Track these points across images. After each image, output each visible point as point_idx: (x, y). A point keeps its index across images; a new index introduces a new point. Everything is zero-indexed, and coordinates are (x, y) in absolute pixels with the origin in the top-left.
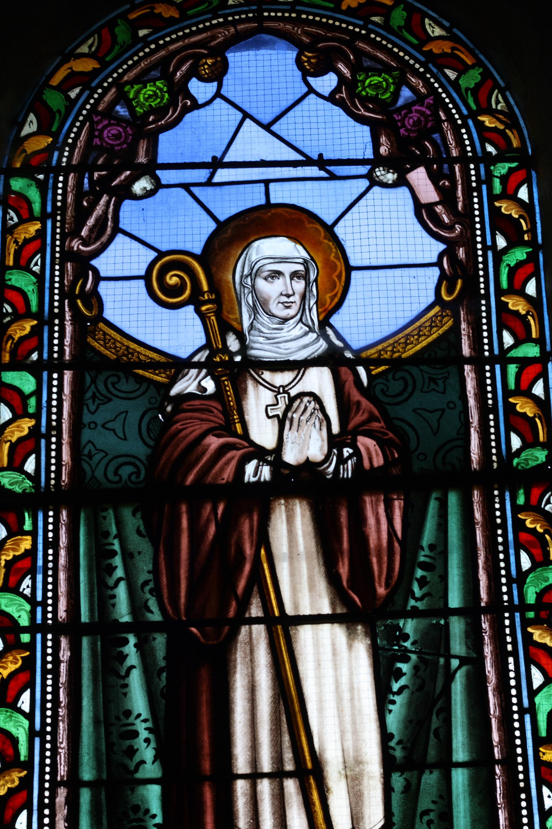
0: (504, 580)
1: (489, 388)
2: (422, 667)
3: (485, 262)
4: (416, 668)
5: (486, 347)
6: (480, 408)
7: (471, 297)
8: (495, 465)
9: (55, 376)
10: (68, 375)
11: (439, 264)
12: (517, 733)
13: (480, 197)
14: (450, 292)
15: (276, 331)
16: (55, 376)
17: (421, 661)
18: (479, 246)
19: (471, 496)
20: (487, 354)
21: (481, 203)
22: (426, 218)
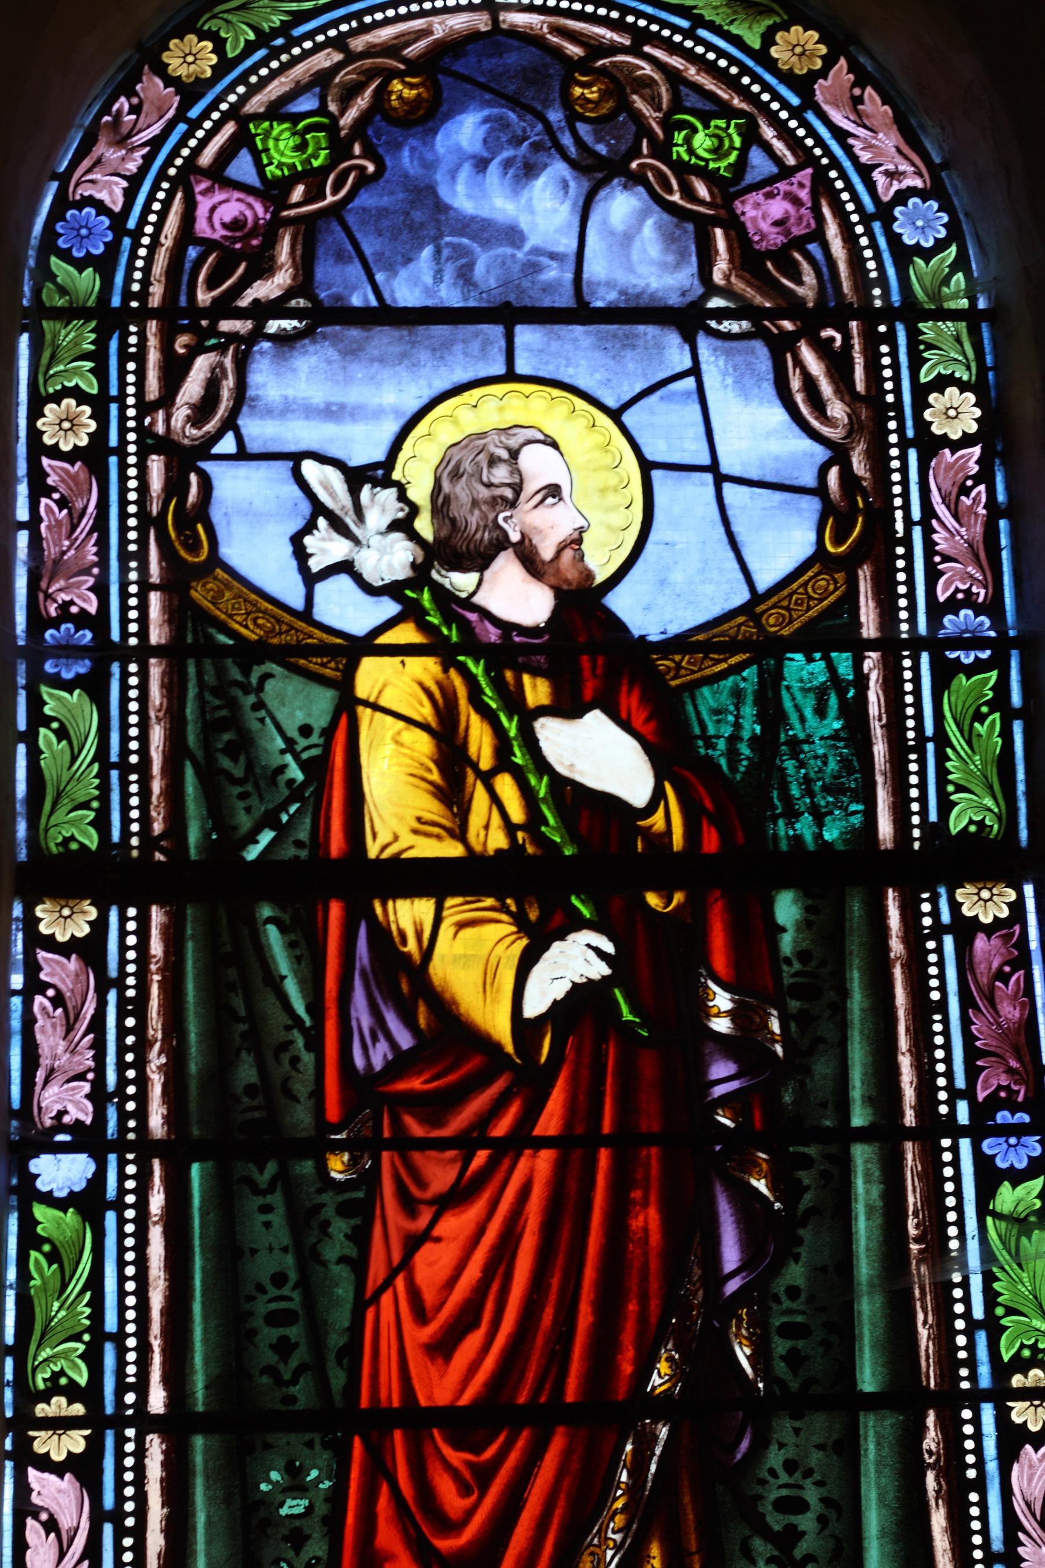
0: (943, 1096)
1: (909, 699)
2: (832, 1516)
3: (904, 470)
4: (822, 1520)
5: (910, 723)
6: (894, 803)
7: (878, 547)
8: (917, 845)
9: (133, 668)
10: (156, 670)
11: (820, 490)
12: (910, 711)
13: (922, 762)
14: (837, 541)
15: (1007, 1267)
16: (133, 668)
17: (827, 1507)
18: (893, 438)
19: (210, 254)
20: (878, 303)
21: (922, 773)
22: (774, 273)
